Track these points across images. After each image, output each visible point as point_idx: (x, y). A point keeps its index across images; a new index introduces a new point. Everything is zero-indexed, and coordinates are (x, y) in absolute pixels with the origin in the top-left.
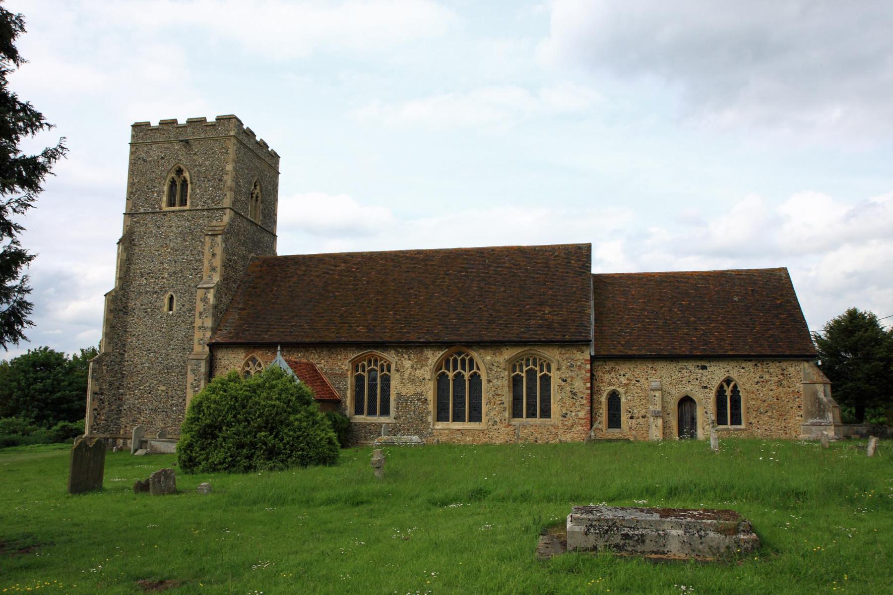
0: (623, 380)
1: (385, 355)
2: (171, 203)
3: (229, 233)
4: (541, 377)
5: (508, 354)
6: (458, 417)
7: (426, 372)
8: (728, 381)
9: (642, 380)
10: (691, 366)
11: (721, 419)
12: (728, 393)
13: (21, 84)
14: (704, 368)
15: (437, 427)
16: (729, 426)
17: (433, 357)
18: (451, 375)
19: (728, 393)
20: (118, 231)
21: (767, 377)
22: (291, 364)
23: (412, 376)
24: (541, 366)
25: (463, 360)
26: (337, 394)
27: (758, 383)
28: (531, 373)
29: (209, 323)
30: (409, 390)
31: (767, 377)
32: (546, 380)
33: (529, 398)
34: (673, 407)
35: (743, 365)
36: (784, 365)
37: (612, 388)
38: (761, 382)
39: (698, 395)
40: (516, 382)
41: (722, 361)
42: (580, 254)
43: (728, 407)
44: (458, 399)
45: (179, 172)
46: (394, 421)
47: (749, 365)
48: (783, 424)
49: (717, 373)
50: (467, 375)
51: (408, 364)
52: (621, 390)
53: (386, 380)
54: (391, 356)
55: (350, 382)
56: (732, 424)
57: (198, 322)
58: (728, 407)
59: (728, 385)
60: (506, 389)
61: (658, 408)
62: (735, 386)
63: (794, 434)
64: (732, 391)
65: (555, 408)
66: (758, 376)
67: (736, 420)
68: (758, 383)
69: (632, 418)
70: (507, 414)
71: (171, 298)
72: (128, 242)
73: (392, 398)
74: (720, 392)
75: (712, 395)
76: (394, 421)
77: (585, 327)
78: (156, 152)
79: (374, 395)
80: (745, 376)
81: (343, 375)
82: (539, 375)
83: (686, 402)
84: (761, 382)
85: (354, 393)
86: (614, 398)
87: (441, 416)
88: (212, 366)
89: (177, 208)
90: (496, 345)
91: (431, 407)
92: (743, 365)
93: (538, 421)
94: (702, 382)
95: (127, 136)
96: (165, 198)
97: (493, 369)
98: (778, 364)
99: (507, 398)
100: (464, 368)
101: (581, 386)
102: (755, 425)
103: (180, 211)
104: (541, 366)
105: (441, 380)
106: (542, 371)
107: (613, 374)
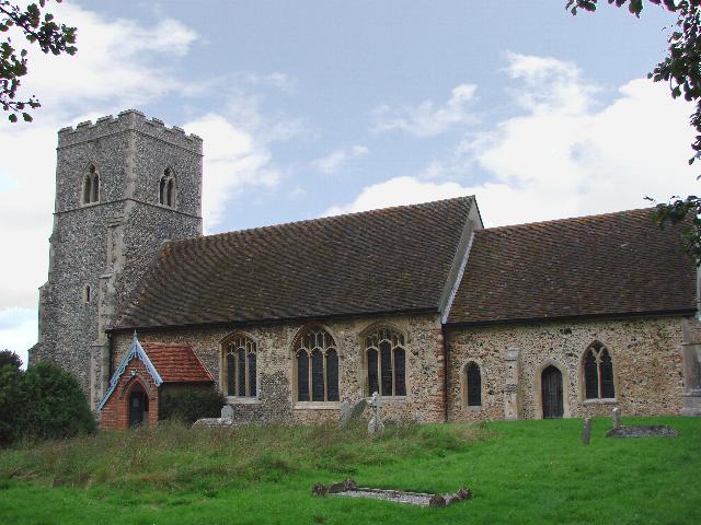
0: (481, 351)
1: (249, 335)
2: (87, 201)
3: (136, 222)
4: (395, 351)
5: (360, 327)
6: (318, 397)
7: (286, 351)
8: (597, 345)
9: (502, 350)
10: (554, 330)
11: (590, 392)
12: (598, 361)
13: (693, 132)
14: (568, 331)
15: (296, 407)
16: (602, 401)
17: (291, 334)
18: (309, 352)
19: (598, 361)
20: (49, 230)
21: (639, 339)
22: (146, 347)
23: (275, 356)
24: (395, 338)
25: (320, 336)
26: (211, 376)
27: (629, 347)
28: (385, 347)
29: (110, 310)
30: (271, 370)
31: (639, 339)
32: (400, 353)
33: (387, 376)
34: (535, 379)
35: (612, 326)
36: (661, 323)
37: (471, 359)
38: (635, 346)
39: (562, 364)
40: (371, 356)
41: (589, 323)
42: (460, 211)
43: (599, 376)
44: (317, 382)
45: (93, 169)
46: (259, 402)
47: (619, 327)
48: (661, 396)
49: (581, 338)
50: (323, 351)
51: (270, 342)
52: (479, 362)
53: (253, 358)
54: (255, 336)
55: (222, 364)
56: (603, 397)
57: (101, 310)
58: (599, 376)
59: (598, 351)
60: (359, 365)
61: (514, 381)
62: (605, 351)
63: (674, 407)
64: (602, 358)
65: (409, 383)
66: (629, 338)
67: (608, 391)
68: (629, 347)
69: (490, 393)
70: (360, 392)
71: (88, 289)
72: (56, 239)
73: (258, 377)
74: (588, 359)
75: (578, 363)
76: (259, 402)
77: (437, 291)
78: (77, 153)
79: (243, 379)
80: (617, 341)
81: (215, 356)
82: (393, 348)
83: (551, 374)
84: (635, 346)
85: (226, 374)
86: (473, 372)
87: (303, 396)
88: (112, 349)
89: (91, 204)
90: (346, 319)
91: (292, 387)
92: (612, 326)
93: (394, 398)
94: (566, 349)
95: (54, 141)
96: (82, 196)
97: (348, 344)
98: (653, 323)
99: (362, 374)
100: (321, 345)
101: (433, 359)
102: (632, 400)
103: (93, 206)
104: (395, 338)
105: (301, 358)
106: (396, 344)
107: (470, 344)
